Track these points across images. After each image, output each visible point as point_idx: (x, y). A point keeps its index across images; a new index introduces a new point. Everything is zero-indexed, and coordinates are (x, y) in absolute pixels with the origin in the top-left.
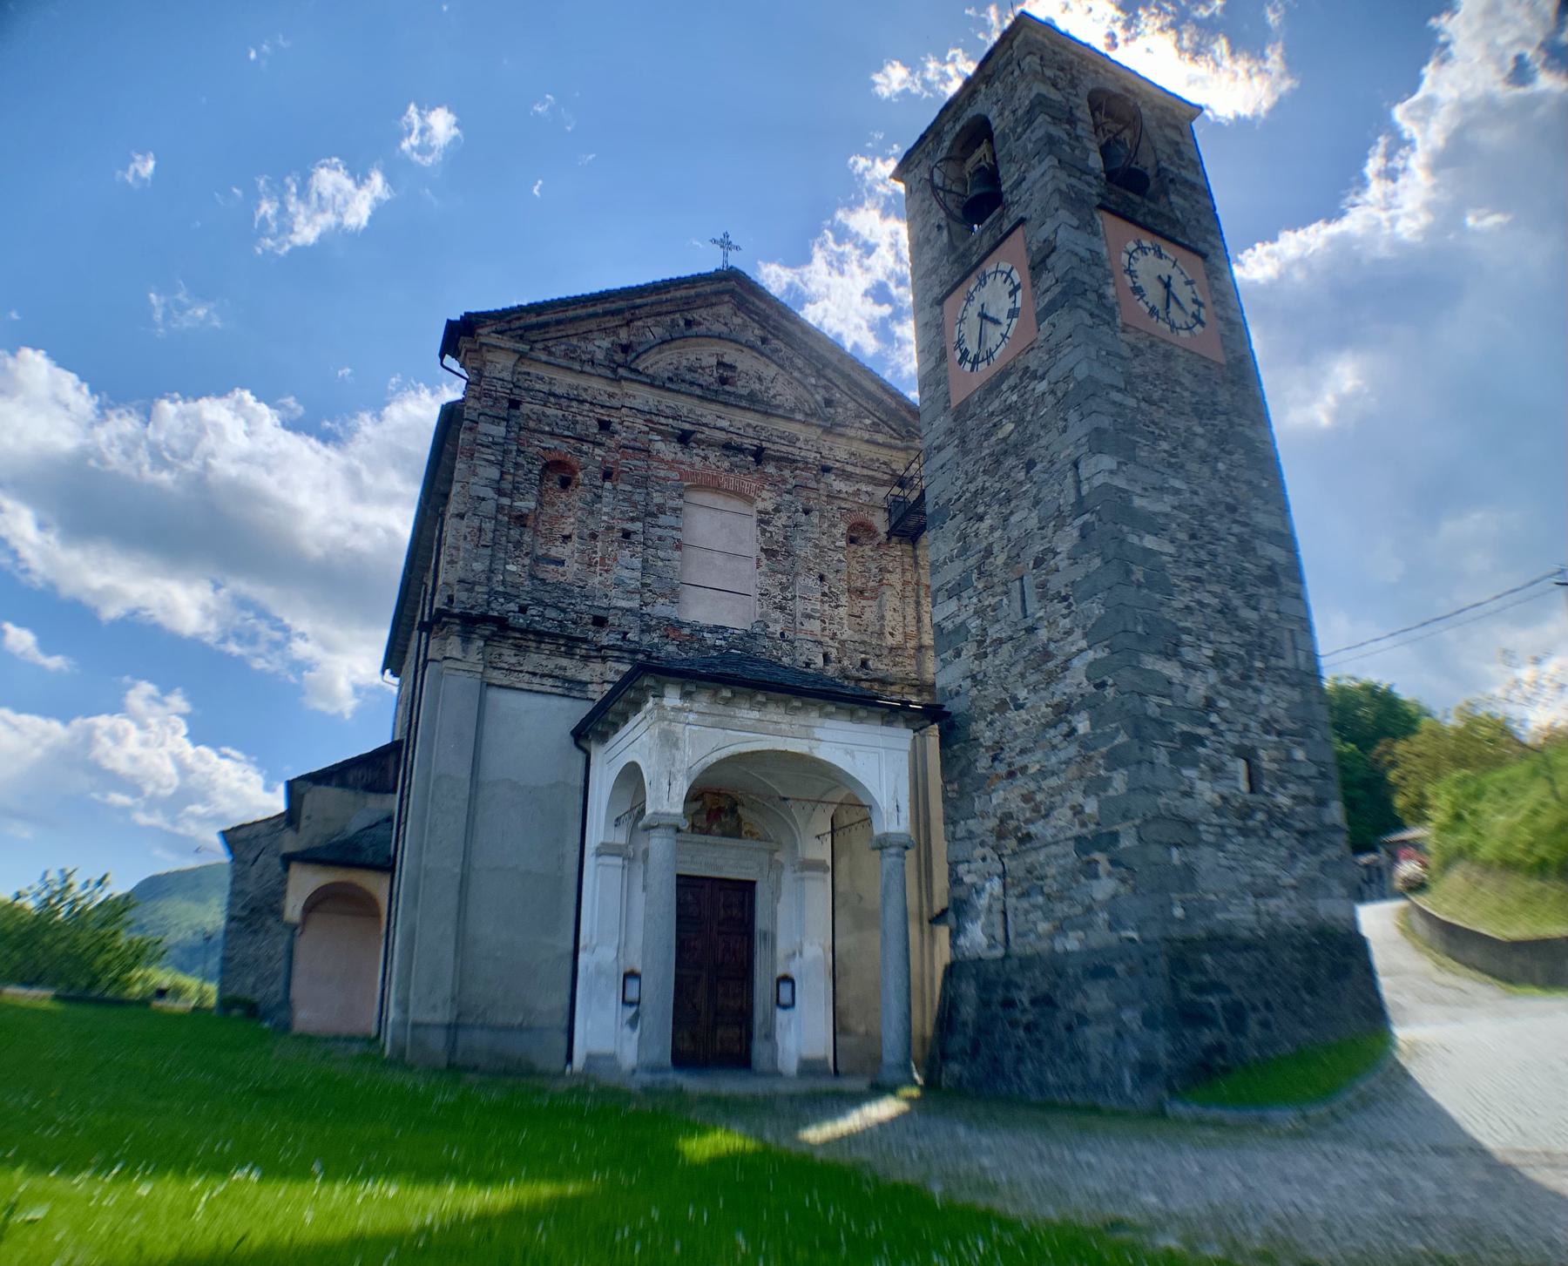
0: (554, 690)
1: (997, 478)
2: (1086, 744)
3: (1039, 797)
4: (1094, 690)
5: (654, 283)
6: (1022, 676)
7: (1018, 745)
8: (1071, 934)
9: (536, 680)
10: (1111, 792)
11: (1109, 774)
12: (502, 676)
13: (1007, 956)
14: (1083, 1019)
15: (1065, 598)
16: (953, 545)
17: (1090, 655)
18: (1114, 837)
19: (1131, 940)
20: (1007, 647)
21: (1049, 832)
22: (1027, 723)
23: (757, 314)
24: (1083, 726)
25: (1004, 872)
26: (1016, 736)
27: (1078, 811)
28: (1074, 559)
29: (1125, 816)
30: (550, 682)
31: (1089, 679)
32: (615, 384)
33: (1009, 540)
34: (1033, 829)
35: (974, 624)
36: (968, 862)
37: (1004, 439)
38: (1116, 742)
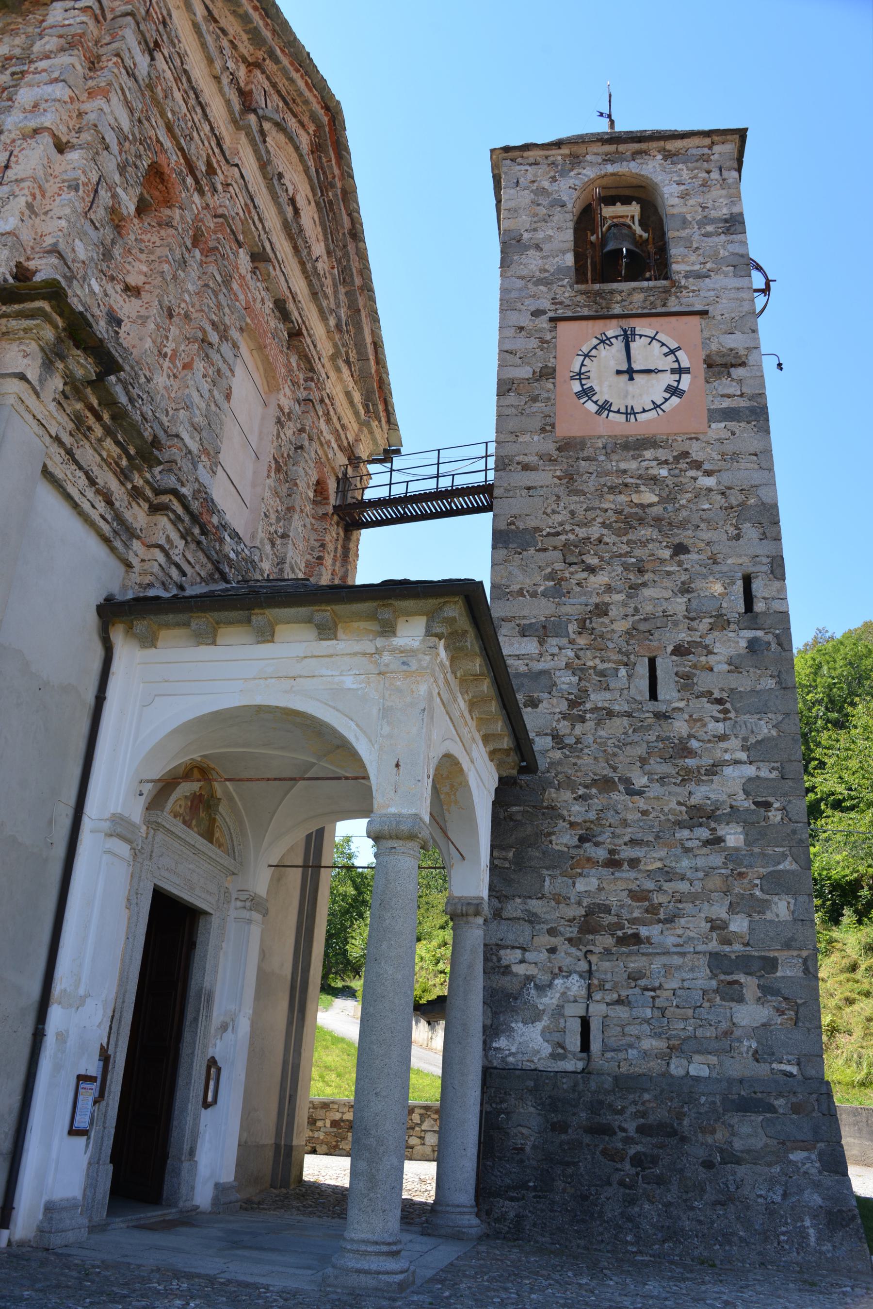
0: (102, 523)
1: (625, 539)
2: (733, 857)
3: (657, 898)
4: (753, 807)
5: (303, 46)
6: (643, 761)
7: (628, 834)
8: (697, 1058)
9: (90, 493)
10: (769, 916)
11: (767, 897)
12: (58, 459)
13: (586, 1072)
14: (732, 1158)
15: (720, 701)
16: (537, 579)
17: (750, 771)
18: (771, 964)
19: (790, 1075)
20: (619, 725)
21: (670, 940)
22: (645, 813)
23: (324, 173)
24: (734, 837)
25: (590, 972)
26: (625, 823)
27: (717, 926)
28: (735, 666)
29: (787, 945)
30: (101, 506)
31: (746, 793)
32: (231, 127)
33: (636, 610)
34: (644, 931)
35: (566, 681)
36: (524, 949)
37: (642, 506)
38: (781, 867)
